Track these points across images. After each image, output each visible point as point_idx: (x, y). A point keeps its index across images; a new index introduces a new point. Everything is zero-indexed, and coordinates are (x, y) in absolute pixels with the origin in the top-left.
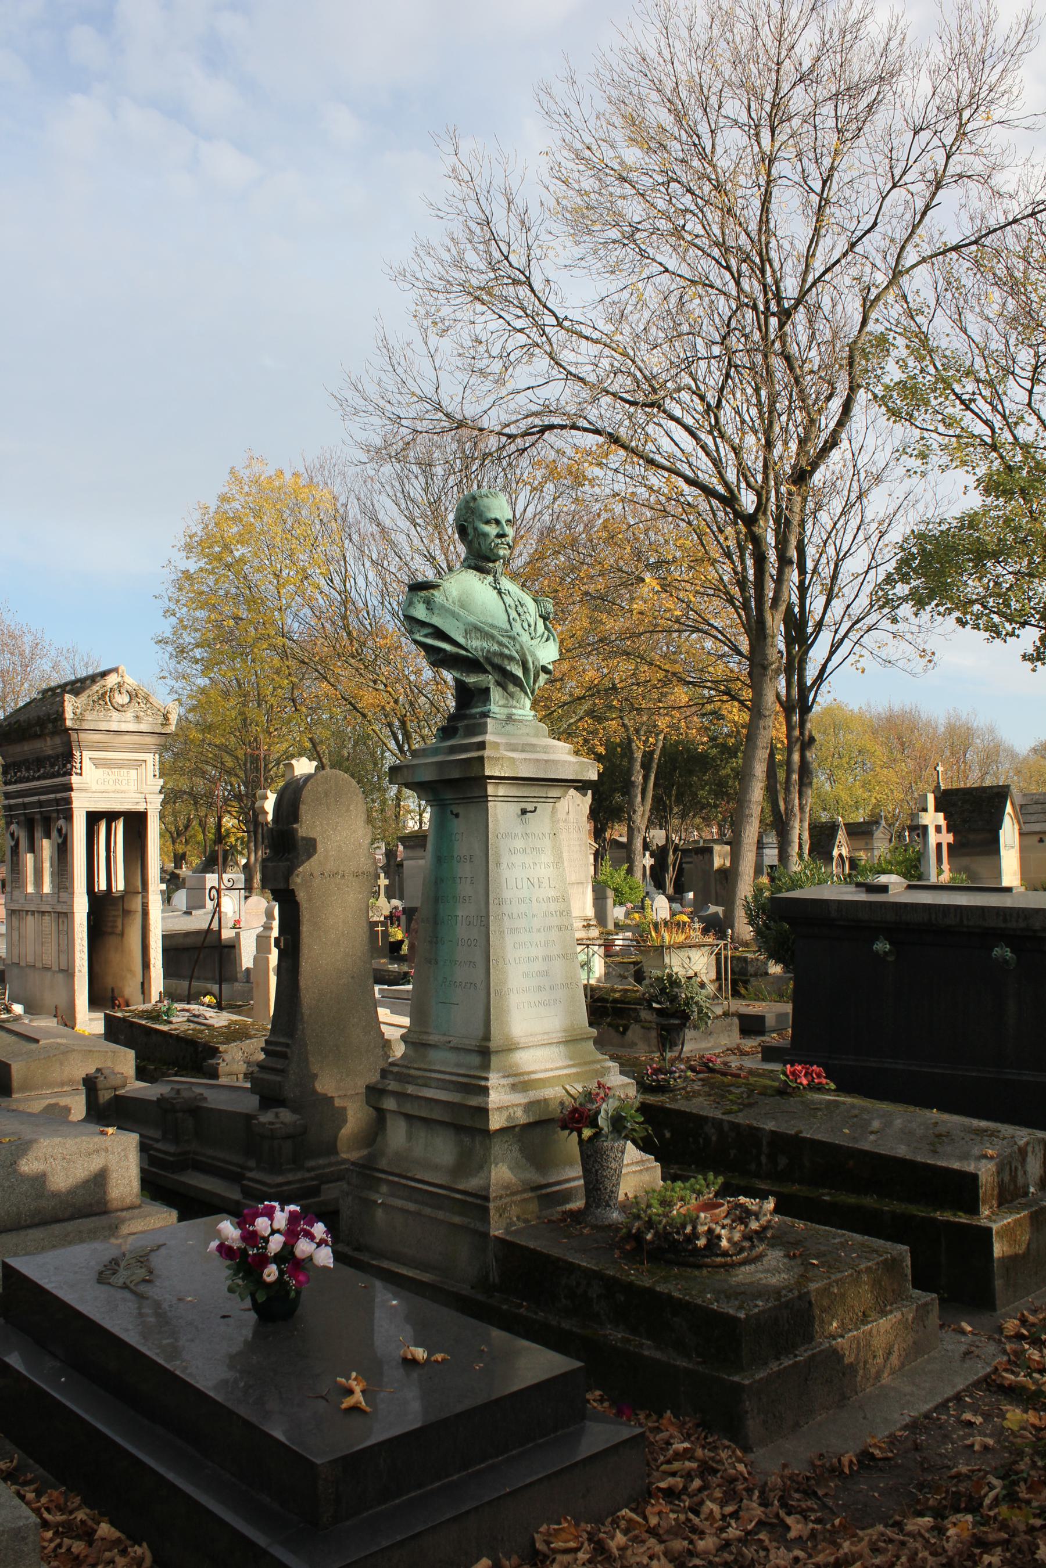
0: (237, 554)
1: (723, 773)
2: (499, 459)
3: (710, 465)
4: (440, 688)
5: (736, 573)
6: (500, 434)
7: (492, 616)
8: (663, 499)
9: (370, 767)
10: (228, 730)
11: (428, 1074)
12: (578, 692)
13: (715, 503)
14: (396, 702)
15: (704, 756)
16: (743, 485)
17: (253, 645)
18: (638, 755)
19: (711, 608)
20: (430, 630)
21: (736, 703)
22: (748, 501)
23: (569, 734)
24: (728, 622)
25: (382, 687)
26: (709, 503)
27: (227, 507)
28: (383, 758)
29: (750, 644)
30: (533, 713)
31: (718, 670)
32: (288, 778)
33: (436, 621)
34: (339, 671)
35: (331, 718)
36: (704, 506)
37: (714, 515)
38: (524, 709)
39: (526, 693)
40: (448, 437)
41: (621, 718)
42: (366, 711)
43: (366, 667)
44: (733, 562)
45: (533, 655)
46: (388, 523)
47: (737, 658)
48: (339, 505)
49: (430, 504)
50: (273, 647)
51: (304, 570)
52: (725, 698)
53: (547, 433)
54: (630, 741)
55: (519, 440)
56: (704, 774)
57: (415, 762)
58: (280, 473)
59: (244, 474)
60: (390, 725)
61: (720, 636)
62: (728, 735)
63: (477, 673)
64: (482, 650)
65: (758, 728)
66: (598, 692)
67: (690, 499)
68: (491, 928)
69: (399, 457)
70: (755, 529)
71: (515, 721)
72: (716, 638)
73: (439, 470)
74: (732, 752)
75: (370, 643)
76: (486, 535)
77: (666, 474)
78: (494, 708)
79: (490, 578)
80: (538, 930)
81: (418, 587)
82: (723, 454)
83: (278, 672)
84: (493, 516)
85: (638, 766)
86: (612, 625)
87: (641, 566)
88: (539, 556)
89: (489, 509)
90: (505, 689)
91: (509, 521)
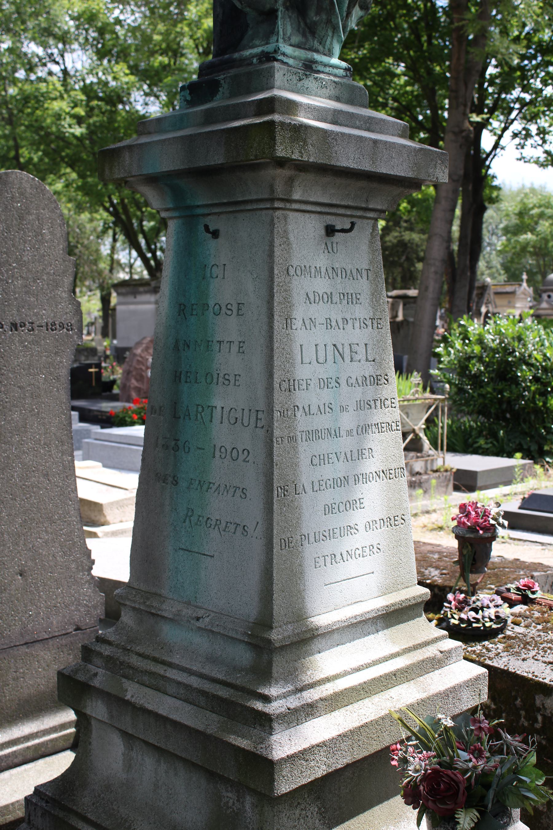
11: (160, 669)
68: (277, 433)
80: (349, 433)
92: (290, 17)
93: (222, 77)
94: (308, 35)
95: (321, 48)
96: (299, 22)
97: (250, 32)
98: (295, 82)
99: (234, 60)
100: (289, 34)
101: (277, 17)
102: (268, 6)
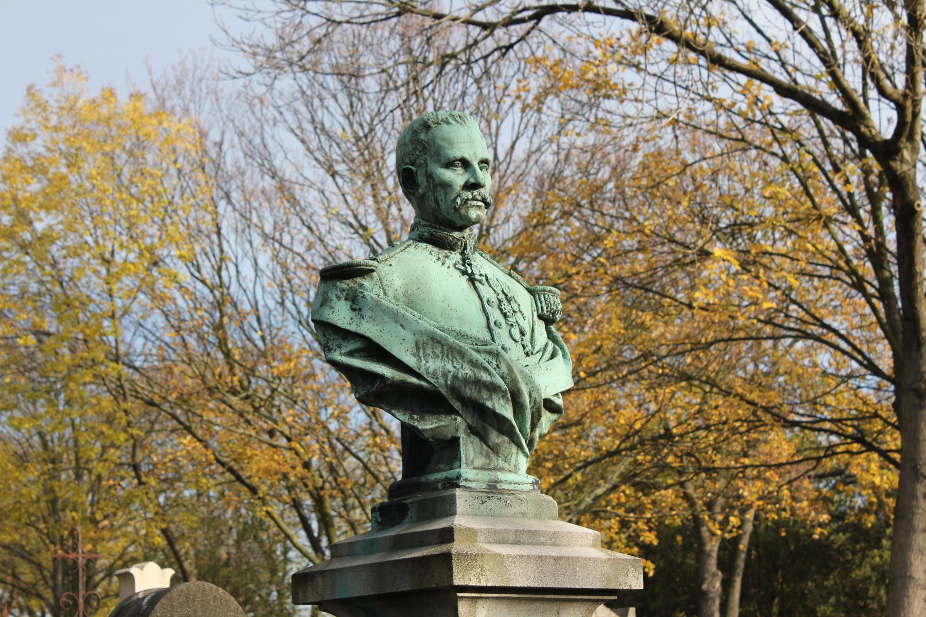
0: (39, 227)
1: (857, 574)
2: (468, 63)
3: (816, 61)
4: (373, 440)
5: (866, 239)
6: (468, 22)
7: (460, 319)
8: (739, 121)
9: (265, 576)
10: (25, 519)
12: (610, 443)
13: (826, 123)
14: (307, 465)
15: (824, 546)
16: (873, 93)
17: (68, 378)
18: (713, 547)
19: (825, 299)
20: (357, 345)
21: (875, 456)
22: (882, 119)
23: (596, 515)
24: (856, 320)
25: (283, 442)
26: (817, 124)
27: (21, 150)
28: (287, 560)
29: (896, 356)
30: (531, 478)
31: (841, 402)
32: (124, 596)
33: (368, 328)
34: (211, 416)
35: (199, 495)
36: (807, 128)
37: (826, 144)
38: (517, 471)
39: (519, 446)
40: (383, 30)
41: (682, 485)
42: (255, 481)
43: (256, 410)
44: (859, 221)
45: (529, 381)
46: (288, 172)
47: (873, 380)
48: (209, 144)
49: (358, 139)
50: (100, 379)
51: (151, 250)
52: (856, 447)
53: (546, 18)
54: (697, 522)
55: (499, 32)
56: (826, 577)
57: (336, 565)
58: (110, 94)
59: (50, 95)
60: (297, 505)
61: (843, 345)
62: (865, 510)
63: (439, 414)
64: (445, 375)
65: (914, 496)
66: (642, 442)
67: (785, 120)
69: (301, 64)
70: (896, 165)
71: (502, 492)
72: (837, 348)
73: (371, 84)
74: (872, 539)
75: (262, 369)
76: (446, 186)
77: (743, 79)
78: (466, 472)
79: (456, 256)
81: (338, 274)
82: (837, 42)
83: (110, 420)
84: (458, 154)
85: (712, 564)
86: (661, 331)
87: (706, 232)
88: (538, 221)
89: (451, 143)
90: (484, 439)
91: (484, 162)
93: (410, 501)
95: (506, 466)
97: (435, 457)
99: (421, 484)
101: (459, 444)
102: (449, 436)
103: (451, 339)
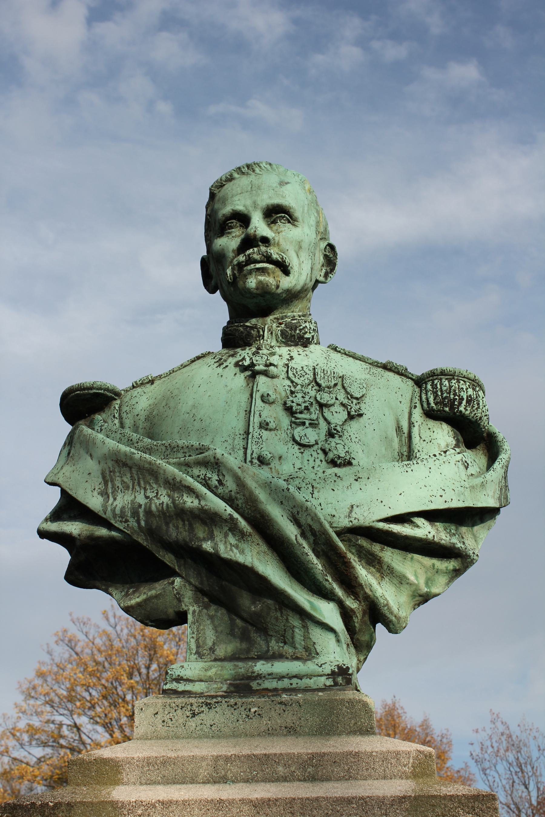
92: (211, 618)
94: (254, 635)
95: (288, 649)
96: (371, 591)
98: (181, 721)
100: (210, 643)
102: (171, 611)
103: (138, 455)
